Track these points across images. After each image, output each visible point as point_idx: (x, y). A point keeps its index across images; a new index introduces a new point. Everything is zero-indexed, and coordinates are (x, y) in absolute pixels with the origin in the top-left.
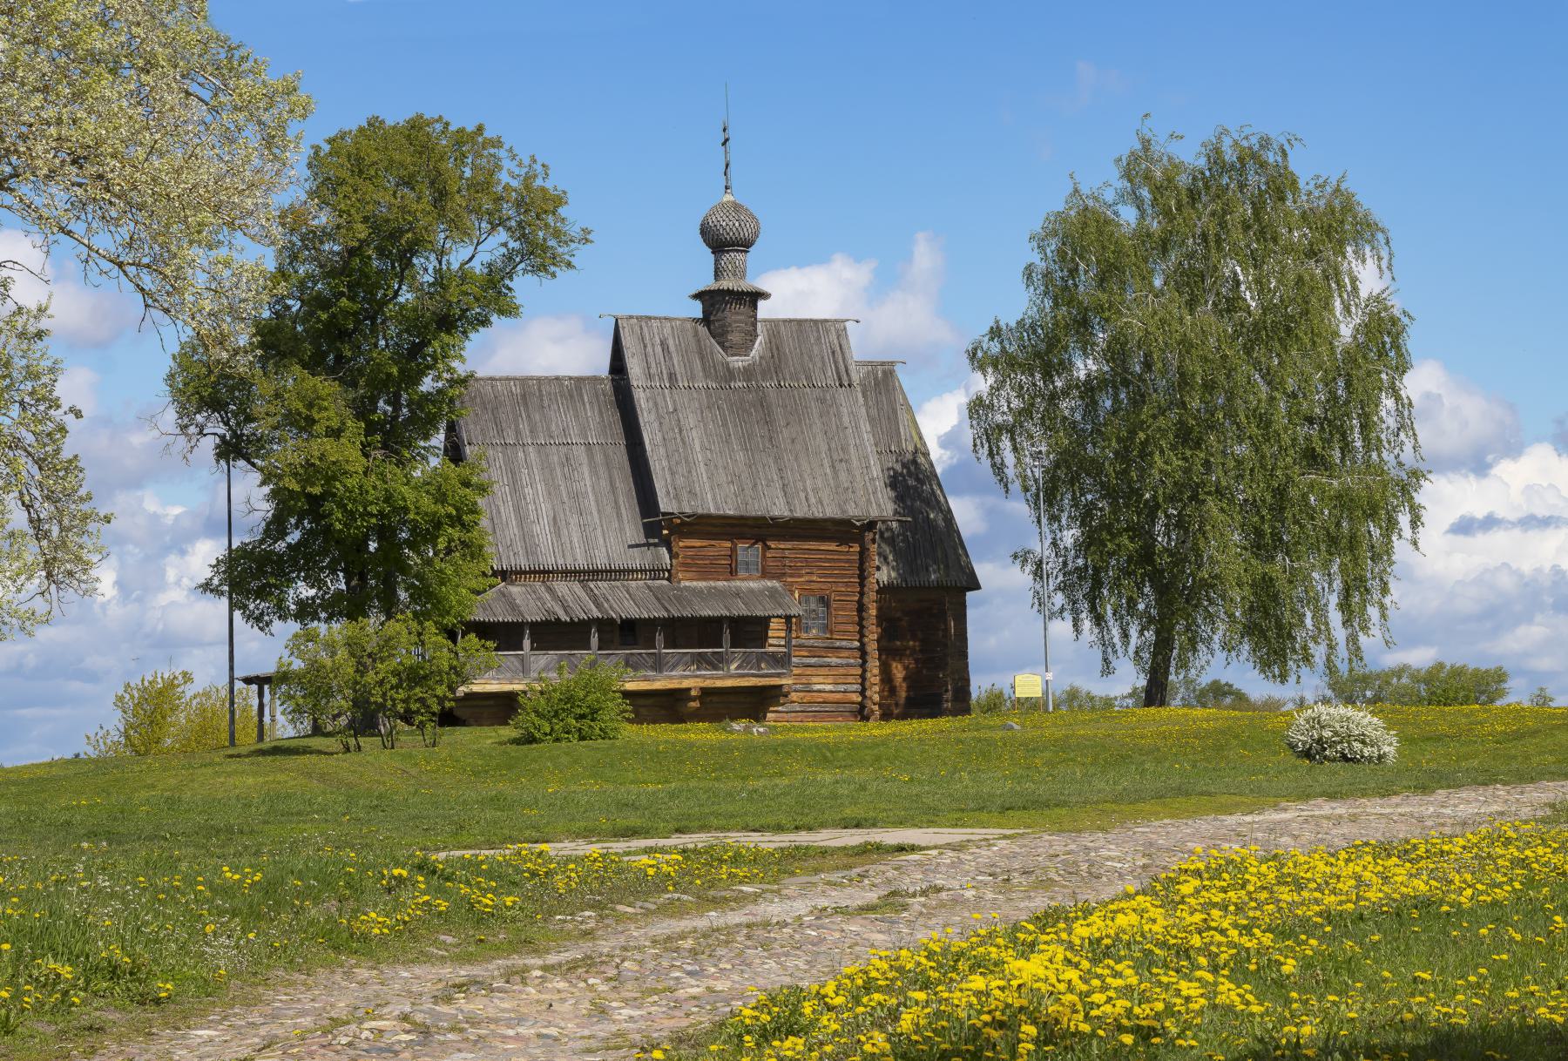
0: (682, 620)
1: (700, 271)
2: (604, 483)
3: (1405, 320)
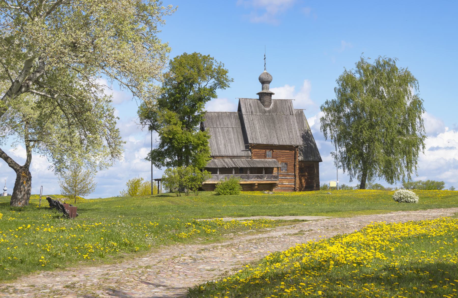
0: (253, 168)
1: (259, 88)
2: (236, 136)
3: (422, 101)
